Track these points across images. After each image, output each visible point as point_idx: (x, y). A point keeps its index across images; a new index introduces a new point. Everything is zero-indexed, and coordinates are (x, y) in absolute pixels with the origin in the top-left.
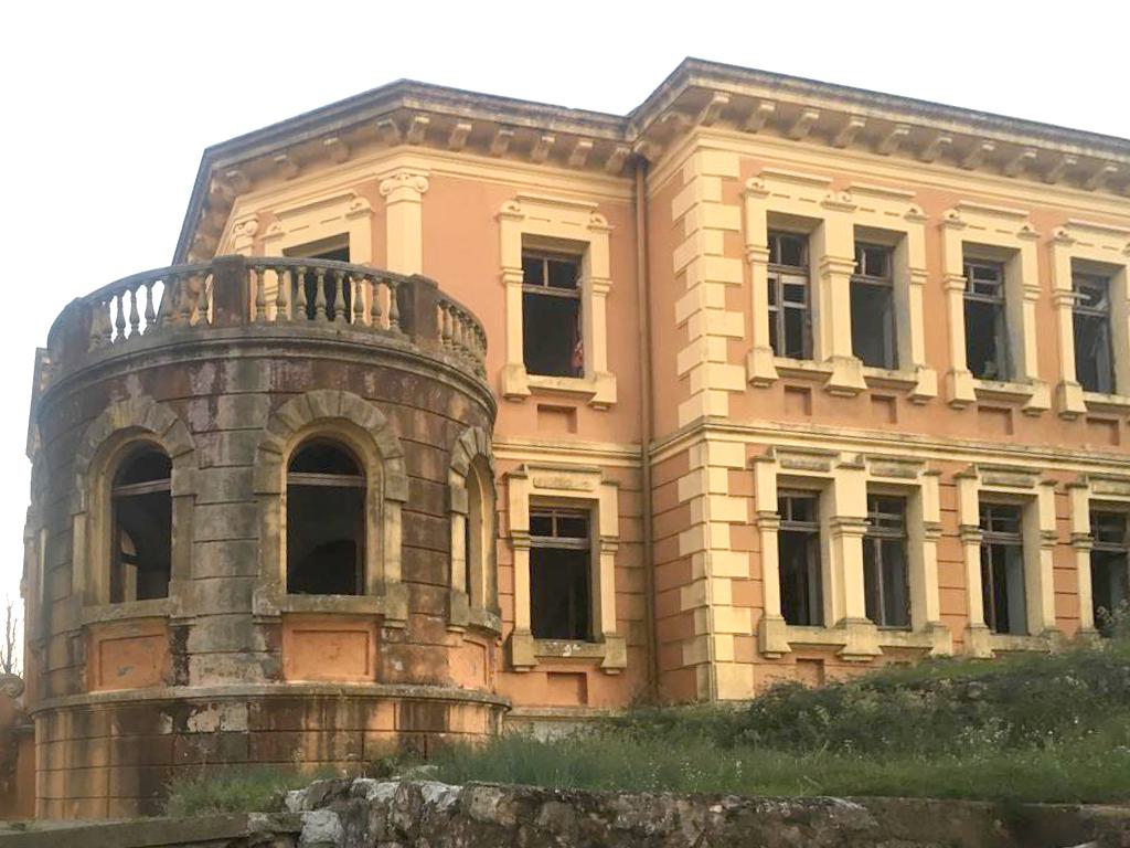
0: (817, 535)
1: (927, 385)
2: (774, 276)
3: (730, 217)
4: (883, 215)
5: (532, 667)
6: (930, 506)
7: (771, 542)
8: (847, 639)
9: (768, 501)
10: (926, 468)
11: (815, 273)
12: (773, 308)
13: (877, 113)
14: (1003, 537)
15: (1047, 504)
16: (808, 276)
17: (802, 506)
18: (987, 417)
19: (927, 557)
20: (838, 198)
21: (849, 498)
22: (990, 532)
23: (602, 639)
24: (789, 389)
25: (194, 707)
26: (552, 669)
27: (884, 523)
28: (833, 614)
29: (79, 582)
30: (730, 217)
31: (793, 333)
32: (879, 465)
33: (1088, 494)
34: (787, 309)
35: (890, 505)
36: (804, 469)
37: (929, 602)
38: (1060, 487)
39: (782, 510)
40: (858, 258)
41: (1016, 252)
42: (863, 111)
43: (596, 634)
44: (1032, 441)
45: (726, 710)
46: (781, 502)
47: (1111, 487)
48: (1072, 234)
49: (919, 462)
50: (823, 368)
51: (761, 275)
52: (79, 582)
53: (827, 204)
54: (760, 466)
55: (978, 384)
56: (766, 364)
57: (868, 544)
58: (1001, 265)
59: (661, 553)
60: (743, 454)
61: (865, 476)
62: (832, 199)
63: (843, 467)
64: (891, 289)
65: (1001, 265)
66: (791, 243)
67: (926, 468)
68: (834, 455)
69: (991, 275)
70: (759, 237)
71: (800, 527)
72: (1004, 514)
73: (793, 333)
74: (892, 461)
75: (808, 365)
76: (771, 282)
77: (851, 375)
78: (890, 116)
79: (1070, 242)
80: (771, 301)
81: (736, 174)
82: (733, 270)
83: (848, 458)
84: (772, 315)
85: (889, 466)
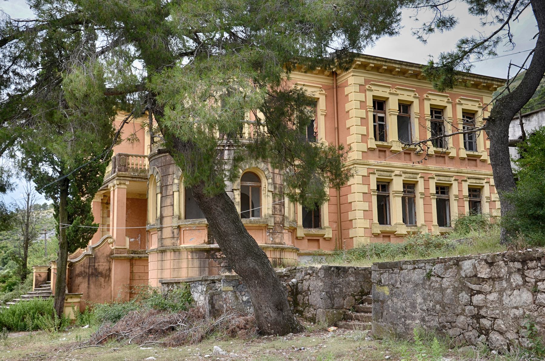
0: (389, 196)
1: (453, 153)
2: (375, 113)
3: (361, 97)
4: (406, 96)
5: (303, 237)
6: (420, 188)
7: (374, 200)
8: (397, 229)
9: (374, 186)
10: (420, 175)
11: (387, 114)
12: (375, 124)
13: (404, 67)
14: (444, 197)
15: (455, 185)
16: (385, 113)
17: (383, 186)
18: (438, 158)
19: (420, 203)
20: (393, 91)
21: (397, 186)
22: (440, 195)
23: (324, 229)
24: (380, 151)
25: (290, 196)
26: (309, 238)
27: (408, 192)
28: (393, 222)
29: (176, 212)
30: (361, 97)
31: (380, 132)
32: (406, 174)
33: (468, 183)
34: (379, 124)
35: (409, 187)
36: (385, 176)
37: (420, 219)
38: (460, 181)
39: (378, 189)
40: (400, 110)
41: (446, 107)
42: (399, 66)
43: (323, 226)
44: (451, 167)
45: (361, 247)
46: (378, 186)
47: (474, 181)
48: (462, 102)
49: (418, 174)
50: (480, 154)
51: (371, 115)
52: (176, 212)
53: (390, 93)
54: (371, 175)
55: (435, 149)
56: (373, 143)
57: (403, 199)
58: (442, 110)
59: (342, 200)
60: (366, 171)
61: (402, 178)
62: (392, 92)
63: (396, 175)
64: (410, 117)
65: (442, 110)
66: (380, 104)
67: (420, 175)
68: (392, 172)
69: (440, 113)
70: (370, 103)
71: (384, 194)
72: (443, 190)
73: (380, 132)
74: (410, 173)
75: (385, 144)
76: (374, 116)
77: (397, 146)
78: (407, 68)
79: (462, 104)
80: (374, 122)
81: (363, 83)
82: (362, 113)
83: (397, 172)
84: (375, 126)
85: (409, 175)
